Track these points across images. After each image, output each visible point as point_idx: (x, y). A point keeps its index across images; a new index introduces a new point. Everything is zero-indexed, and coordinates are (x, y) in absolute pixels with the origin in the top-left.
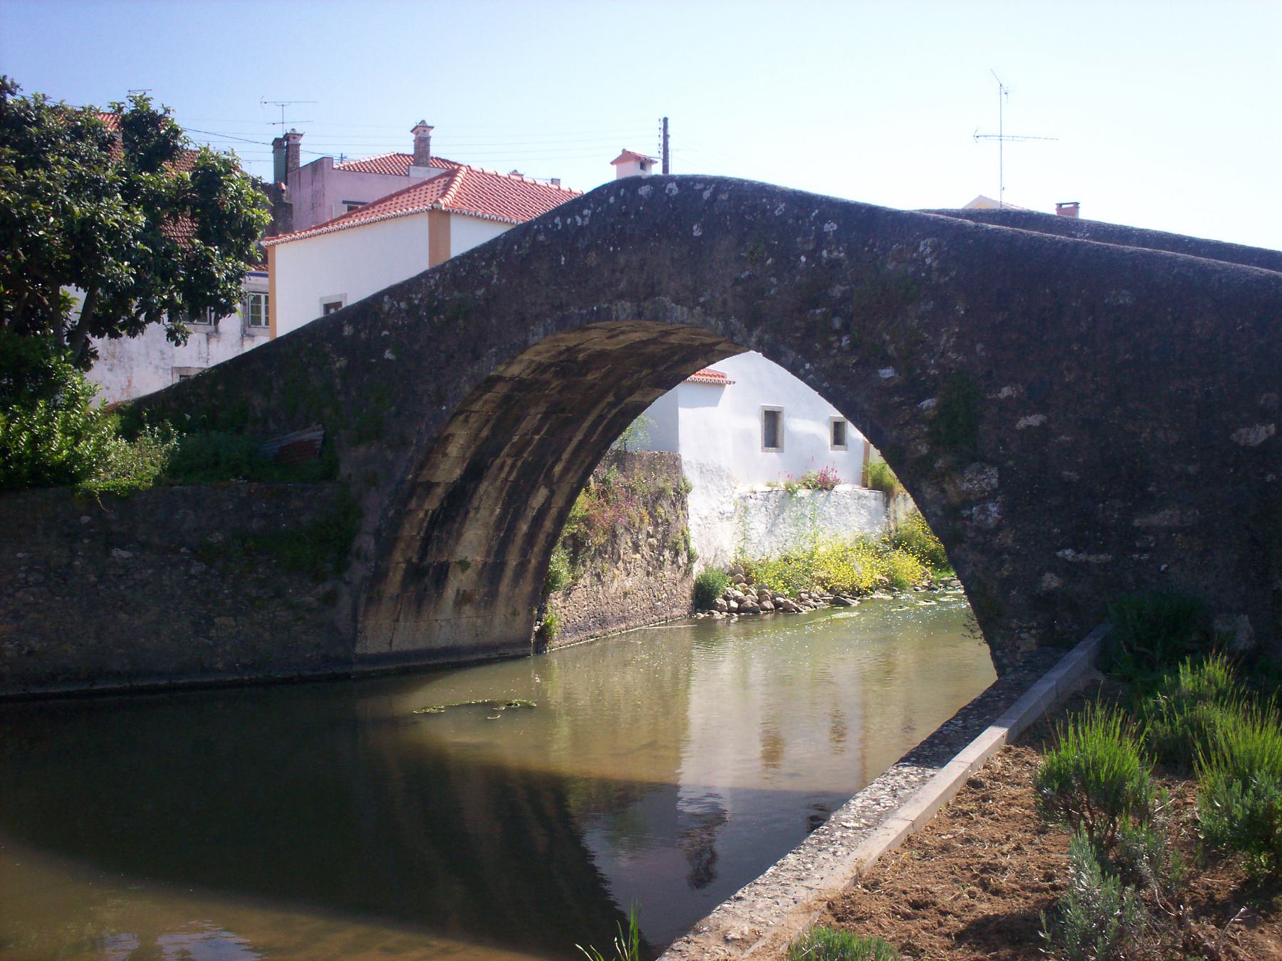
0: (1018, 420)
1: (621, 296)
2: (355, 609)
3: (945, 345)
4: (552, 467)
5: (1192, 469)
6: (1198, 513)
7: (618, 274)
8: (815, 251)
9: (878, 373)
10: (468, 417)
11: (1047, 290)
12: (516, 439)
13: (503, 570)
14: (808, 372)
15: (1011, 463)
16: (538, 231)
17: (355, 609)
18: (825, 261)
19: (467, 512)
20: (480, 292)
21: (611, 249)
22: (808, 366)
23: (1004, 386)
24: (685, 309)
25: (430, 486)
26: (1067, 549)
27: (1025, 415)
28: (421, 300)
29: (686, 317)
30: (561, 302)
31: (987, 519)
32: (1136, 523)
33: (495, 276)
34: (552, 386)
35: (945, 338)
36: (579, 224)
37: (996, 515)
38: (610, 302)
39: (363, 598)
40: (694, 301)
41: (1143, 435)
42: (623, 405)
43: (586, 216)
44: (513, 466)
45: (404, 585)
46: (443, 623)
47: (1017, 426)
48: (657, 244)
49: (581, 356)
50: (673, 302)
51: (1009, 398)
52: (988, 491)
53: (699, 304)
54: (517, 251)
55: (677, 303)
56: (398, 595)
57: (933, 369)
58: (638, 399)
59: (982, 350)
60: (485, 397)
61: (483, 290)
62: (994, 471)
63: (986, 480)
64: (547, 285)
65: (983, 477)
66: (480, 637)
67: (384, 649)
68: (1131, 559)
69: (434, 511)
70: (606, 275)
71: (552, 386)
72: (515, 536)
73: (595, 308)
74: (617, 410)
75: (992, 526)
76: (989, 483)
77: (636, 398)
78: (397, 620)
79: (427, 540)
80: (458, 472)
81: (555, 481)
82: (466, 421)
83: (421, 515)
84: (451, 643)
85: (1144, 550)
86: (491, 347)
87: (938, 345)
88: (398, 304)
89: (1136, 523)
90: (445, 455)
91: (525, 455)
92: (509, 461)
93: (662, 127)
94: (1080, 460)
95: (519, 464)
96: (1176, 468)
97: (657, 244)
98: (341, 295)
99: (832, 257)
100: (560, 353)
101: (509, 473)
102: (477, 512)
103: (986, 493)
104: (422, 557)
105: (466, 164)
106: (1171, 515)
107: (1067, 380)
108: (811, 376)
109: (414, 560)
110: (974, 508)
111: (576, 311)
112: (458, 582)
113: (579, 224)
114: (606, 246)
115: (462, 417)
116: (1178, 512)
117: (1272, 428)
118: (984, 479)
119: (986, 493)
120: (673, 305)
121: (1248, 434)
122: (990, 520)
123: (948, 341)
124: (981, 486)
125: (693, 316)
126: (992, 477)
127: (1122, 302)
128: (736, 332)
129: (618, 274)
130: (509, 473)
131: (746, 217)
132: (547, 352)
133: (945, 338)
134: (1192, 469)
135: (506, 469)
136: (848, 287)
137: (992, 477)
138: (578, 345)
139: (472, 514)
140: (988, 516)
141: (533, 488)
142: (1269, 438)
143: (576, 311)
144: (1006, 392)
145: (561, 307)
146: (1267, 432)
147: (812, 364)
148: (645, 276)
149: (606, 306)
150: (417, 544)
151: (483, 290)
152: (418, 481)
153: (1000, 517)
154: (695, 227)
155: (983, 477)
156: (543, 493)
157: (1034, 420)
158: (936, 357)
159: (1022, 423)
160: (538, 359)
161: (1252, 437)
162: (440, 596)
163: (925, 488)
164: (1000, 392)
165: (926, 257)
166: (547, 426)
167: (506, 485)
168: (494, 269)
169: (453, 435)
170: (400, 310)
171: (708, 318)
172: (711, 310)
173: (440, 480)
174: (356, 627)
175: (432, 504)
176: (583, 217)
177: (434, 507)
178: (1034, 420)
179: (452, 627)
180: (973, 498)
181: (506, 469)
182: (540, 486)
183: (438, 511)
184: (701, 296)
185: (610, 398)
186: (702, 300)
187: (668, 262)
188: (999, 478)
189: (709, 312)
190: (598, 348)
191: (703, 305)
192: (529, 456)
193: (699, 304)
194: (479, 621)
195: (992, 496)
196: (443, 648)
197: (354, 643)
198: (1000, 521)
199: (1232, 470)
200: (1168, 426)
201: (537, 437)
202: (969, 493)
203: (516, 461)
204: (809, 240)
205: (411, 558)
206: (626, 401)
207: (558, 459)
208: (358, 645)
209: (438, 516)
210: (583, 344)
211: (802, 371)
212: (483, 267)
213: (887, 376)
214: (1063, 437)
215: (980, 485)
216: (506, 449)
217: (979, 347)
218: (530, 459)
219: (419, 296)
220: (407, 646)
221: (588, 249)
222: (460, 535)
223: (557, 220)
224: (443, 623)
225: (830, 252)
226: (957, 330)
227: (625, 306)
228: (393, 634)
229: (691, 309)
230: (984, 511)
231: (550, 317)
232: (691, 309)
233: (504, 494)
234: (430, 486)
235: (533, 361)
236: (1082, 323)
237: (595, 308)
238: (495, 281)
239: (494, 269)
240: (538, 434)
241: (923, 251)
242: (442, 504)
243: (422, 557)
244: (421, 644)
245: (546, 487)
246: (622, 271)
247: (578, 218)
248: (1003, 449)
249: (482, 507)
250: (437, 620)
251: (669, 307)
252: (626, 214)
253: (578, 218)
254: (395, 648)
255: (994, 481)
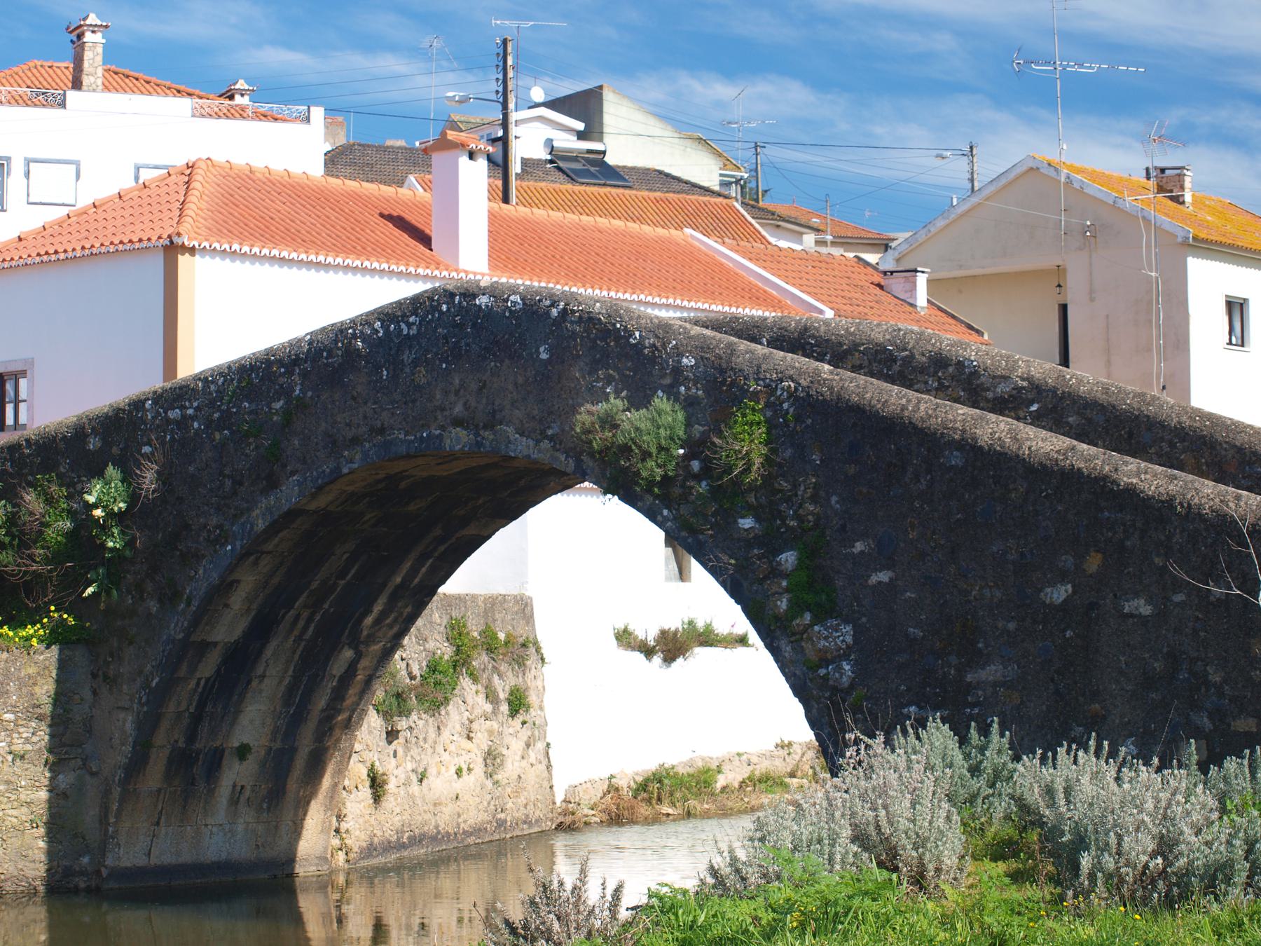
0: (869, 576)
1: (458, 422)
2: (105, 809)
3: (802, 496)
4: (360, 620)
5: (1012, 626)
6: (1016, 667)
7: (452, 398)
8: (671, 386)
9: (738, 523)
10: (257, 559)
11: (893, 446)
12: (315, 585)
13: (292, 760)
14: (666, 519)
15: (864, 620)
16: (354, 336)
17: (105, 809)
18: (683, 398)
19: (249, 682)
20: (278, 405)
21: (444, 366)
22: (665, 512)
23: (858, 541)
24: (531, 443)
25: (205, 647)
26: (912, 706)
27: (876, 570)
28: (197, 409)
29: (531, 451)
30: (383, 424)
31: (841, 677)
32: (969, 678)
33: (298, 388)
34: (365, 519)
35: (802, 488)
36: (405, 332)
37: (850, 673)
38: (443, 428)
39: (116, 792)
40: (541, 434)
41: (974, 593)
42: (454, 539)
43: (413, 324)
44: (310, 620)
45: (168, 776)
46: (215, 830)
47: (869, 581)
48: (498, 364)
49: (403, 485)
50: (517, 433)
51: (862, 552)
52: (843, 649)
53: (547, 437)
54: (327, 358)
55: (522, 435)
56: (159, 791)
57: (792, 520)
58: (474, 532)
59: (837, 502)
60: (281, 535)
61: (281, 403)
62: (848, 629)
63: (841, 638)
64: (366, 403)
65: (838, 634)
66: (261, 849)
67: (141, 861)
68: (965, 713)
69: (208, 680)
70: (438, 397)
71: (365, 519)
72: (308, 713)
73: (425, 435)
74: (446, 545)
75: (846, 685)
76: (843, 641)
77: (471, 530)
78: (158, 824)
79: (197, 719)
80: (238, 632)
81: (362, 639)
82: (256, 563)
83: (193, 683)
84: (224, 856)
85: (973, 705)
86: (293, 473)
87: (796, 495)
88: (166, 413)
89: (969, 678)
90: (227, 606)
91: (326, 606)
92: (306, 614)
93: (501, 89)
94: (923, 617)
95: (318, 618)
96: (1000, 625)
97: (498, 364)
98: (26, 361)
99: (690, 393)
100: (379, 481)
101: (305, 628)
102: (261, 682)
103: (842, 651)
104: (191, 737)
105: (205, 157)
106: (996, 671)
107: (911, 537)
108: (669, 524)
109: (181, 744)
110: (830, 667)
111: (402, 436)
112: (234, 774)
113: (405, 332)
114: (437, 362)
115: (252, 558)
116: (1001, 667)
117: (1069, 587)
118: (839, 636)
119: (842, 651)
120: (517, 436)
121: (1052, 593)
122: (845, 679)
123: (805, 491)
124: (836, 644)
125: (539, 451)
126: (846, 634)
127: (953, 462)
128: (588, 471)
129: (452, 398)
130: (305, 628)
131: (599, 342)
132: (362, 481)
133: (802, 488)
134: (1012, 626)
135: (301, 623)
136: (706, 428)
137: (846, 634)
138: (401, 473)
139: (255, 683)
140: (841, 675)
141: (334, 649)
142: (1068, 597)
143: (402, 436)
144: (859, 547)
145: (382, 431)
146: (1066, 591)
147: (670, 510)
148: (484, 401)
149: (438, 432)
150: (186, 721)
151: (281, 403)
152: (191, 640)
153: (853, 675)
154: (542, 349)
155: (838, 634)
156: (348, 654)
157: (884, 576)
158: (794, 508)
159: (874, 579)
160: (350, 489)
161: (1055, 596)
162: (211, 792)
163: (784, 646)
164: (853, 547)
165: (784, 402)
166: (356, 567)
167: (299, 644)
168: (296, 378)
169: (238, 581)
170: (168, 421)
171: (557, 454)
172: (560, 444)
173: (218, 638)
174: (107, 831)
175: (208, 667)
176: (409, 325)
177: (207, 675)
178: (884, 576)
179: (225, 835)
180: (829, 656)
181: (301, 623)
182: (343, 647)
183: (212, 679)
184: (549, 428)
185: (437, 531)
186: (550, 432)
187: (510, 387)
188: (854, 636)
189: (558, 446)
190: (425, 474)
191: (551, 439)
192: (330, 606)
193: (547, 437)
194: (260, 828)
195: (845, 656)
196: (214, 863)
197: (103, 850)
198: (854, 679)
199: (1041, 627)
200: (992, 584)
201: (342, 582)
202: (825, 650)
203: (313, 614)
204: (666, 373)
205: (176, 741)
206: (458, 535)
207: (368, 611)
208: (109, 855)
209: (213, 686)
210: (407, 471)
211: (659, 518)
212: (282, 375)
213: (746, 526)
214: (908, 594)
215: (836, 642)
216: (301, 600)
217: (834, 499)
218: (332, 610)
219: (195, 404)
220: (168, 859)
221: (415, 363)
222: (238, 712)
223: (378, 324)
224: (215, 830)
225: (688, 389)
226: (814, 480)
227: (460, 434)
228: (152, 841)
229: (538, 442)
230: (839, 668)
231: (369, 442)
232: (538, 442)
233: (297, 657)
234: (205, 647)
235: (345, 491)
236: (922, 481)
237: (425, 435)
238: (297, 392)
239: (296, 378)
240: (343, 578)
241: (781, 395)
242: (218, 671)
243: (191, 737)
244: (186, 858)
245: (350, 647)
246: (457, 393)
247: (403, 326)
248: (857, 606)
249: (268, 674)
250: (206, 825)
251: (512, 438)
252: (461, 326)
253: (403, 326)
254: (154, 861)
255: (849, 639)
